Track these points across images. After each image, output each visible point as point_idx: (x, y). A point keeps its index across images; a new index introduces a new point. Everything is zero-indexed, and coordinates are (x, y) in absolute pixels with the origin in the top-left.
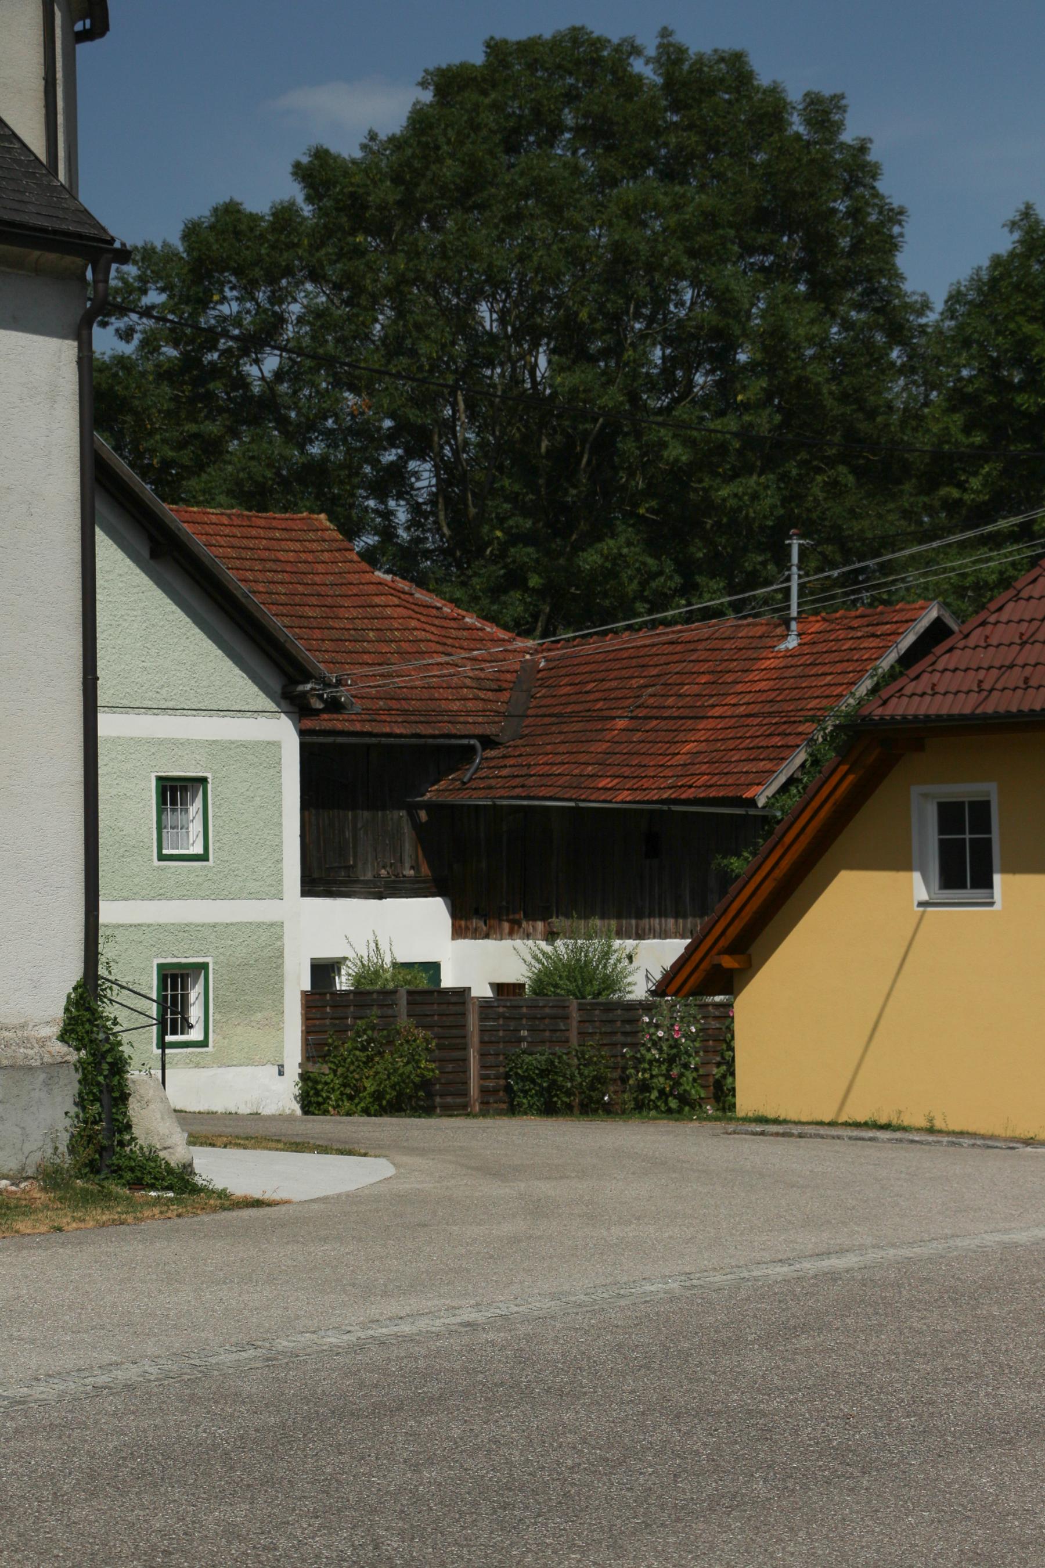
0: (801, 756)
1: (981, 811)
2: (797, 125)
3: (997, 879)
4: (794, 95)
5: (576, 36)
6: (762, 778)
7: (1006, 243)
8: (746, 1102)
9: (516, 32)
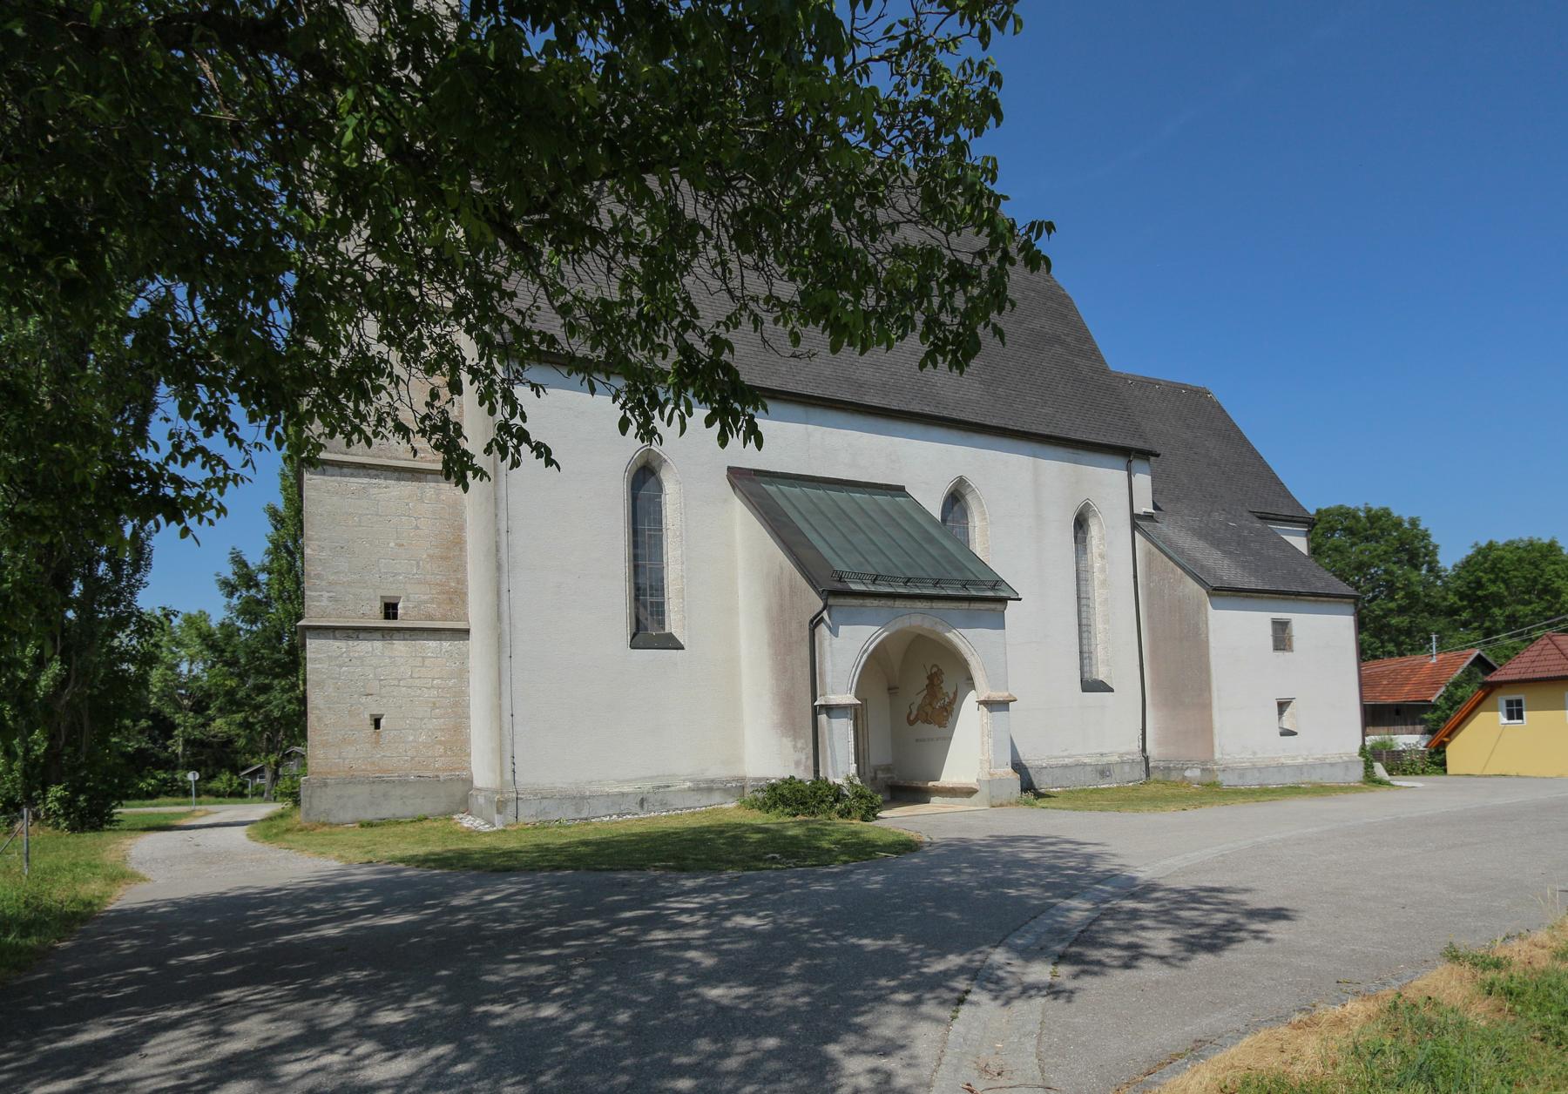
0: (1443, 689)
1: (1519, 703)
2: (1406, 525)
3: (1525, 713)
4: (1406, 518)
5: (1341, 507)
6: (1432, 695)
7: (1470, 552)
8: (1449, 772)
9: (1324, 507)
